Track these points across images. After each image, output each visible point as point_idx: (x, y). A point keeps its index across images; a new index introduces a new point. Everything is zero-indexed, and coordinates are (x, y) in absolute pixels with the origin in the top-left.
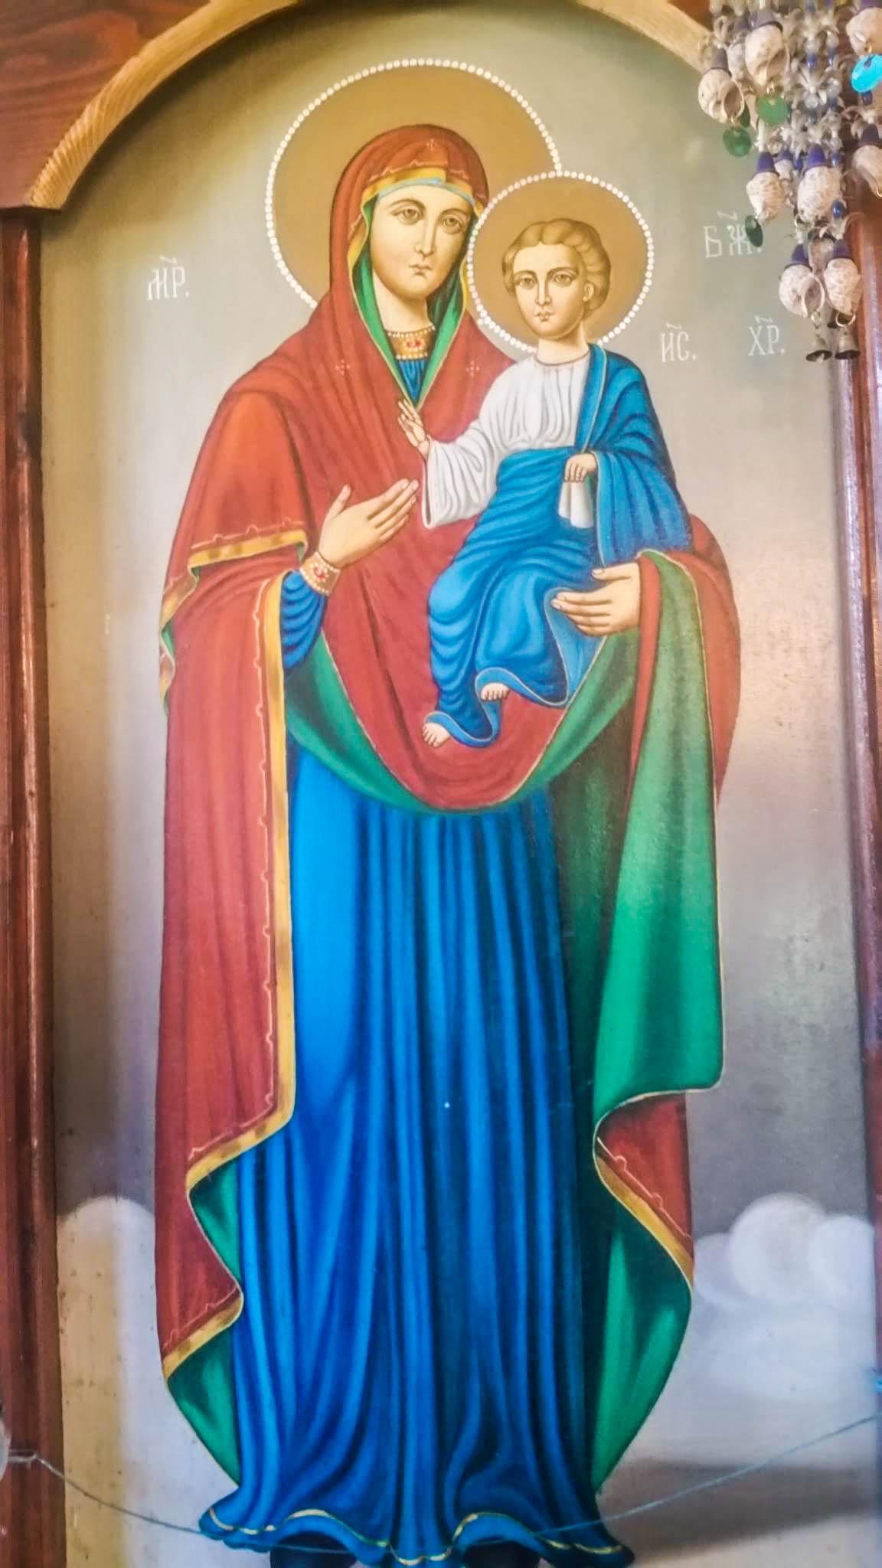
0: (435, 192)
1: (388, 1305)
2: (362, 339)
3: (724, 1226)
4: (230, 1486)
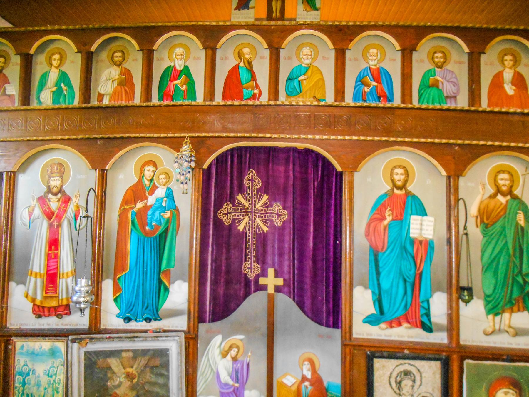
0: (152, 168)
1: (138, 291)
2: (142, 184)
3: (173, 283)
4: (119, 311)
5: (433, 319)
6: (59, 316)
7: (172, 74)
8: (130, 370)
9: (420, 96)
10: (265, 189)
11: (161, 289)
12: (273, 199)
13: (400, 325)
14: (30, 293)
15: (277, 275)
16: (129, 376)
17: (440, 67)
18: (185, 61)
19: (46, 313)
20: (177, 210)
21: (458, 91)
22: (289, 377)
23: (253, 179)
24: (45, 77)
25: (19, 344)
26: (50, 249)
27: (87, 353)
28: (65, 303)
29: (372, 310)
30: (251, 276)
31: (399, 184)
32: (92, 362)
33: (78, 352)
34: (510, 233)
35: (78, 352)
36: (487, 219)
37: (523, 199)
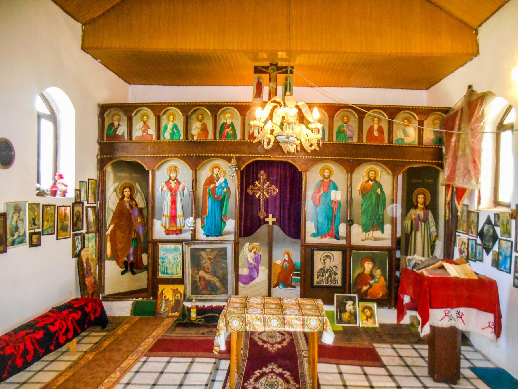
0: (217, 169)
5: (340, 234)
6: (177, 234)
7: (225, 126)
8: (210, 256)
9: (337, 137)
10: (268, 179)
11: (223, 222)
12: (272, 184)
13: (326, 237)
14: (164, 224)
15: (273, 217)
16: (210, 259)
17: (346, 124)
18: (231, 120)
19: (171, 233)
20: (229, 188)
21: (353, 135)
22: (278, 261)
23: (263, 174)
24: (166, 126)
25: (161, 246)
26: (172, 205)
27: (191, 249)
28: (179, 228)
29: (314, 231)
30: (262, 217)
31: (327, 176)
32: (194, 252)
33: (187, 249)
34: (374, 197)
35: (187, 249)
36: (364, 191)
37: (381, 183)
